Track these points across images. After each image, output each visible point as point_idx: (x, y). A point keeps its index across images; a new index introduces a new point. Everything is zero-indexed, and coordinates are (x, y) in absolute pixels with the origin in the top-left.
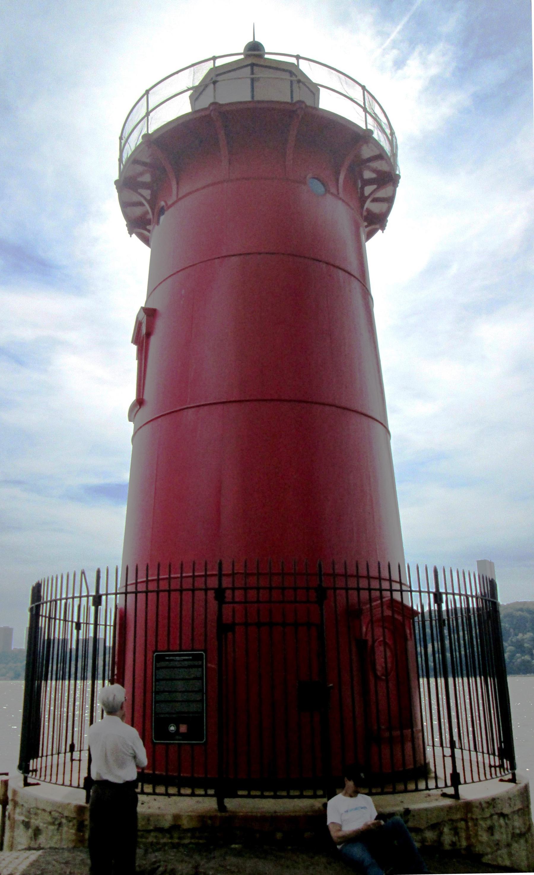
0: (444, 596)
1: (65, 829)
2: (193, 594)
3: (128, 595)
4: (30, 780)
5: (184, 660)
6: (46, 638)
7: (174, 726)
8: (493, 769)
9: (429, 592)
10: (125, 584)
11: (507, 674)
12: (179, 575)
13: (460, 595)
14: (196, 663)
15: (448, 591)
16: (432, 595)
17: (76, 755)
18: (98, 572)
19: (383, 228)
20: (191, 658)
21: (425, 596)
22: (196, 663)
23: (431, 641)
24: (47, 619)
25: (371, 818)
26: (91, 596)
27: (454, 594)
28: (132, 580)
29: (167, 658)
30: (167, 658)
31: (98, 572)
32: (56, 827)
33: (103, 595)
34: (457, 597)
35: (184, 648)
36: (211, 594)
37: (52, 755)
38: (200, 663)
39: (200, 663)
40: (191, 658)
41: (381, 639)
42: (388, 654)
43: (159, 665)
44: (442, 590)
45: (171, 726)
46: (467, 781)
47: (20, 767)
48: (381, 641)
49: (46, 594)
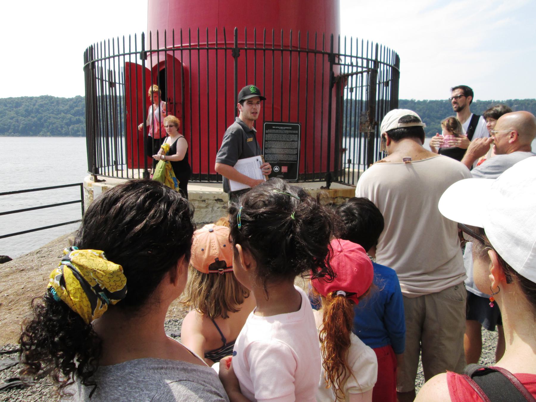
3: (131, 55)
5: (286, 129)
6: (114, 95)
7: (278, 168)
11: (84, 102)
12: (215, 42)
14: (294, 132)
15: (350, 58)
17: (119, 167)
18: (143, 35)
20: (291, 128)
22: (294, 132)
24: (104, 79)
25: (193, 200)
26: (139, 53)
29: (274, 127)
30: (274, 127)
31: (143, 35)
33: (148, 51)
35: (283, 121)
37: (108, 165)
38: (297, 132)
39: (297, 132)
40: (291, 128)
43: (267, 132)
44: (379, 60)
45: (275, 167)
46: (124, 176)
47: (90, 170)
49: (97, 56)
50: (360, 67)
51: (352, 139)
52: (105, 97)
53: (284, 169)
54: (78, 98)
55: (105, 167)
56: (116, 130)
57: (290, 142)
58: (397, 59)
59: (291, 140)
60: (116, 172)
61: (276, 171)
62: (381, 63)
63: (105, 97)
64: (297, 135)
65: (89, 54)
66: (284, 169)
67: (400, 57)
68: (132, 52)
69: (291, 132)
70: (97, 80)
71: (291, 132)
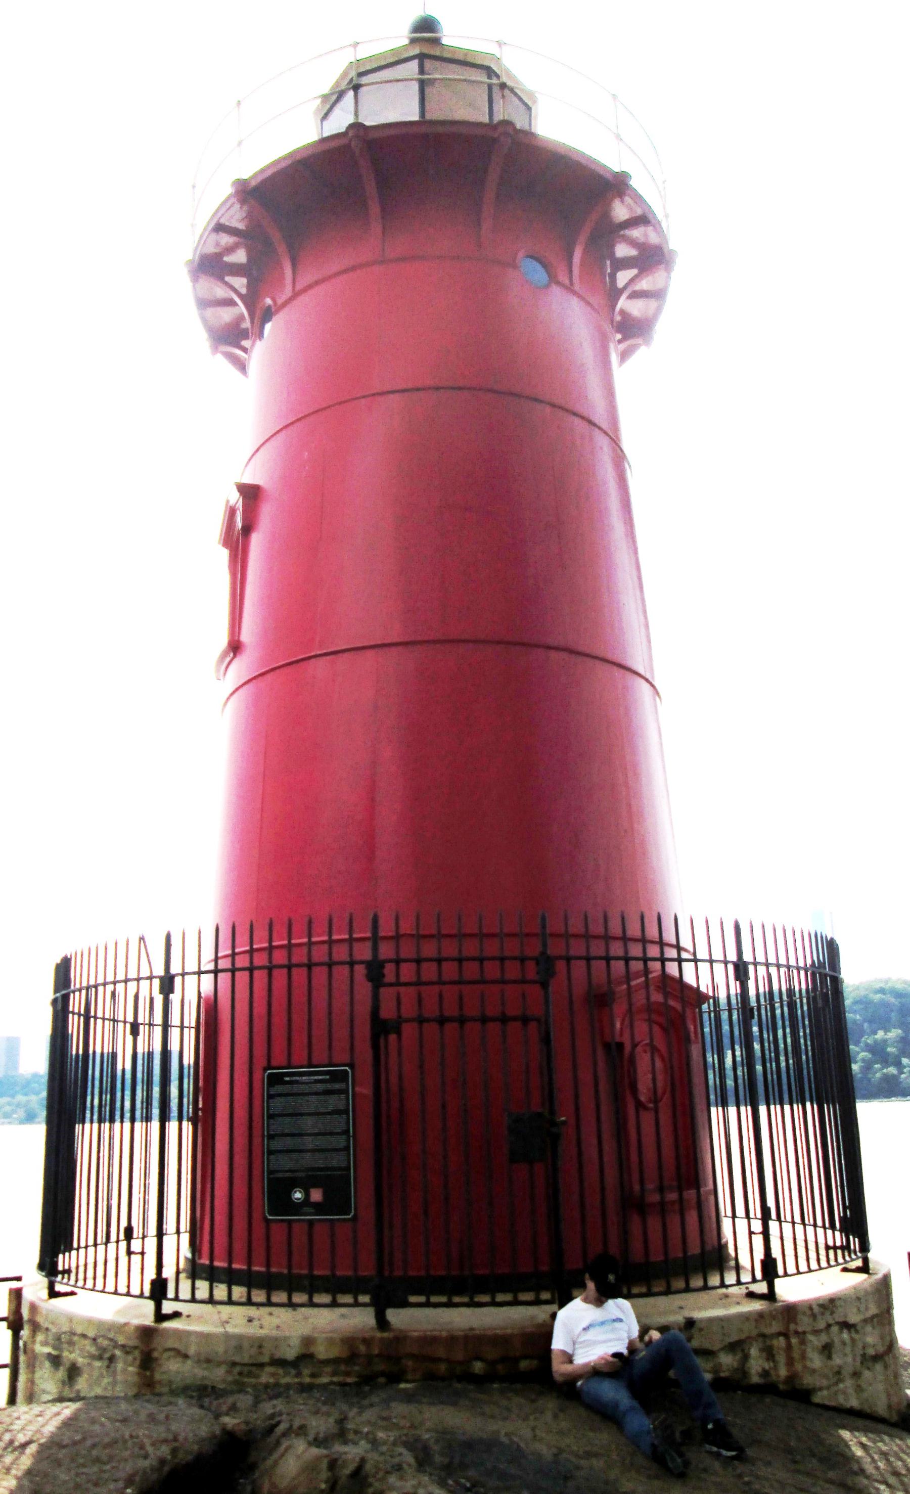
0: (751, 968)
1: (120, 1366)
2: (270, 975)
4: (59, 1288)
7: (300, 1192)
8: (831, 1252)
9: (726, 963)
10: (213, 957)
13: (778, 966)
14: (337, 1086)
16: (731, 967)
18: (168, 938)
21: (719, 968)
22: (337, 1086)
23: (706, 1035)
27: (767, 965)
28: (224, 951)
29: (287, 1079)
31: (168, 938)
32: (106, 1363)
34: (773, 970)
36: (360, 970)
41: (647, 1041)
42: (659, 1064)
44: (747, 957)
48: (646, 1044)
50: (784, 966)
51: (787, 1108)
52: (814, 1098)
53: (316, 1195)
54: (36, 1076)
55: (95, 1245)
56: (146, 1156)
57: (329, 1117)
58: (832, 948)
59: (330, 1108)
60: (189, 1282)
61: (297, 1199)
62: (755, 964)
63: (814, 1098)
64: (343, 1096)
65: (63, 971)
66: (316, 1195)
67: (839, 941)
68: (118, 979)
69: (329, 1086)
70: (71, 1015)
71: (329, 1086)
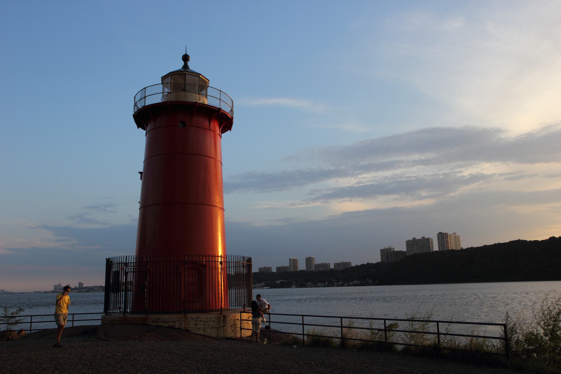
19: (230, 130)
65: (290, 259)
